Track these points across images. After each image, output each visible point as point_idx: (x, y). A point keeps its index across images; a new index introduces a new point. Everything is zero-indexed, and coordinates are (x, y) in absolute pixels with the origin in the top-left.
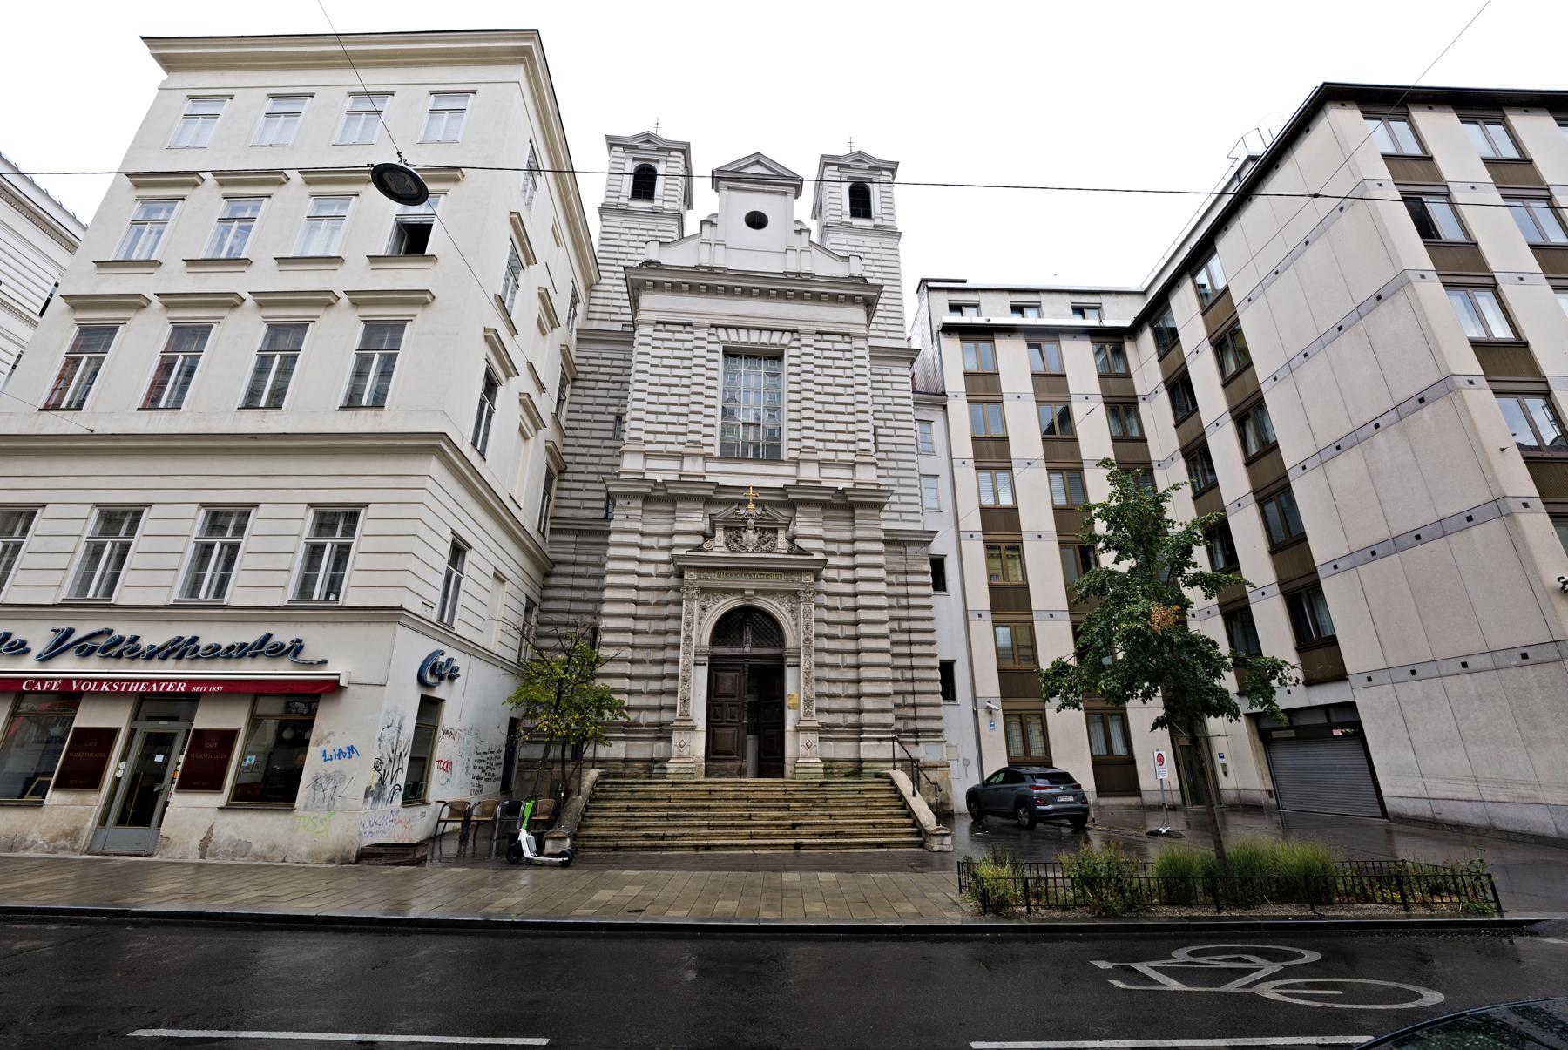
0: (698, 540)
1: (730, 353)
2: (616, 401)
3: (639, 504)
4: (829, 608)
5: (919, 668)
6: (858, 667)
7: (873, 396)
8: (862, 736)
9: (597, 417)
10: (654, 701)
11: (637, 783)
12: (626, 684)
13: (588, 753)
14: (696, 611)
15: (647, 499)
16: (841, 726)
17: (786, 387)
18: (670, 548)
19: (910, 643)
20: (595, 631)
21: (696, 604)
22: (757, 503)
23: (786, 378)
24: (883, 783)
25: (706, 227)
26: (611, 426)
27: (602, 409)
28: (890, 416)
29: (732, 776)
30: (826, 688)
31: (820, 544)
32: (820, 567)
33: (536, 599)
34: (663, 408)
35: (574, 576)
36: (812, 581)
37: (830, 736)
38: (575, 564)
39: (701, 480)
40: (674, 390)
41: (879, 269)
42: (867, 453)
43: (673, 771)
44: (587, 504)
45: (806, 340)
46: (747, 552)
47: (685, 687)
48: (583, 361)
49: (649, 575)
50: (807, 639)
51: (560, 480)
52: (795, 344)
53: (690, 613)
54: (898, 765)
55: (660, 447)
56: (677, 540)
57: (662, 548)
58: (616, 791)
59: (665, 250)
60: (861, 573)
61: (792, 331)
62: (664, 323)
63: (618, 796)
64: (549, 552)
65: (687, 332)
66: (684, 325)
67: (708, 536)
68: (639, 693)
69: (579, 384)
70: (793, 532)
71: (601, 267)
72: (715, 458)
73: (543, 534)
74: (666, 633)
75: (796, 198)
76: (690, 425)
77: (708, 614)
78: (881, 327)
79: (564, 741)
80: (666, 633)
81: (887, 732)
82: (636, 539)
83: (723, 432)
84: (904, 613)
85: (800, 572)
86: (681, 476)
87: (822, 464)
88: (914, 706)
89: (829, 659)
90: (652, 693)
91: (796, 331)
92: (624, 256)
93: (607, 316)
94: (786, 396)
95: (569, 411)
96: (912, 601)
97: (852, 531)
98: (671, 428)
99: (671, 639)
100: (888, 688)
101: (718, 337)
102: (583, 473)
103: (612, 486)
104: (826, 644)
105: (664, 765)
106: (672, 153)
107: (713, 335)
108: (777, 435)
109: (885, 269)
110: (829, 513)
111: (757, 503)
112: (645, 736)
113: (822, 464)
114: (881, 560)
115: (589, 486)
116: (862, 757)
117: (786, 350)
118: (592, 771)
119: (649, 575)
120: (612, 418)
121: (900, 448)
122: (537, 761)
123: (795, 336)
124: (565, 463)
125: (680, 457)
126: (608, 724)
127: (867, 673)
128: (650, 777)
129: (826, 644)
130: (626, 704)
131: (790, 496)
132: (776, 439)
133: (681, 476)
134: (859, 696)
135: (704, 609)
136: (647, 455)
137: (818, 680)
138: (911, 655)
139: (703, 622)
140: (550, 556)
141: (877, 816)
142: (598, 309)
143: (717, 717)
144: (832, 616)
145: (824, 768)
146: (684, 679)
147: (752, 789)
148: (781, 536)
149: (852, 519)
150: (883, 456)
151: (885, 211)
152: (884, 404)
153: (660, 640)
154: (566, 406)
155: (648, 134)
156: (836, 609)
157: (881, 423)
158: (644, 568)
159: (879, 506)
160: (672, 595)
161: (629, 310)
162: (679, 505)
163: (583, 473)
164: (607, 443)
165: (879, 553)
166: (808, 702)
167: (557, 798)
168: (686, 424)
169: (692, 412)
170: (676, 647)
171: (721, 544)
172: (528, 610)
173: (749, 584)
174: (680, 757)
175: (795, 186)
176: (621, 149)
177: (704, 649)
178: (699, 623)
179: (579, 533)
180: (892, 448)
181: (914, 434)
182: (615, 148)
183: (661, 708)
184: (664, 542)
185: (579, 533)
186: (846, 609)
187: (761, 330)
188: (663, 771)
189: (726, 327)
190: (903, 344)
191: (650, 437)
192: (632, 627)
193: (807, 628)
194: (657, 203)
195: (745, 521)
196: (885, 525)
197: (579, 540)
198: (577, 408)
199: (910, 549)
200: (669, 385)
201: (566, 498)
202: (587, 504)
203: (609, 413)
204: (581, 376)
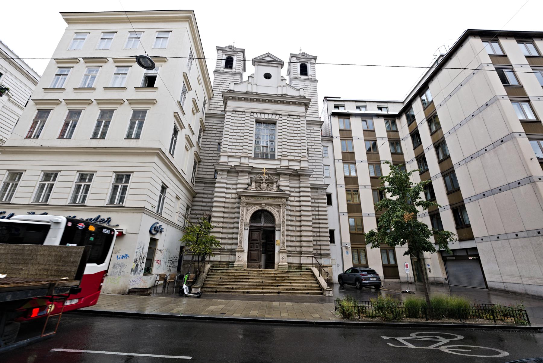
0: (246, 186)
1: (258, 122)
3: (226, 173)
4: (291, 211)
5: (322, 232)
6: (301, 231)
8: (302, 255)
9: (212, 143)
10: (230, 241)
11: (224, 270)
12: (220, 235)
13: (207, 259)
14: (245, 210)
15: (228, 172)
16: (295, 252)
17: (277, 134)
18: (236, 189)
19: (319, 223)
20: (210, 217)
21: (245, 208)
22: (266, 174)
23: (277, 131)
25: (250, 78)
26: (216, 146)
27: (214, 140)
28: (313, 144)
30: (289, 238)
31: (288, 188)
33: (190, 206)
36: (285, 201)
37: (291, 255)
38: (203, 193)
39: (247, 165)
41: (310, 93)
42: (305, 157)
43: (236, 266)
44: (208, 173)
45: (284, 118)
47: (241, 237)
48: (207, 124)
50: (283, 221)
51: (199, 165)
52: (280, 119)
53: (243, 211)
54: (314, 266)
55: (233, 154)
56: (239, 186)
57: (233, 189)
58: (216, 272)
59: (236, 86)
60: (302, 198)
61: (280, 115)
62: (235, 111)
63: (217, 274)
64: (195, 189)
65: (243, 114)
67: (249, 185)
68: (225, 238)
69: (206, 132)
71: (214, 92)
74: (234, 218)
76: (244, 146)
77: (249, 212)
78: (310, 113)
79: (199, 254)
80: (234, 218)
81: (311, 254)
82: (225, 185)
83: (255, 149)
84: (317, 213)
85: (281, 198)
86: (240, 164)
87: (289, 160)
88: (320, 245)
89: (290, 228)
90: (229, 239)
91: (281, 114)
93: (216, 109)
94: (277, 137)
95: (202, 141)
96: (320, 209)
97: (299, 184)
98: (237, 148)
99: (236, 220)
100: (311, 239)
101: (254, 116)
102: (207, 162)
103: (217, 167)
104: (290, 223)
105: (233, 263)
106: (239, 53)
107: (252, 115)
110: (292, 178)
111: (266, 174)
112: (227, 253)
113: (289, 160)
114: (309, 194)
117: (277, 121)
118: (208, 265)
120: (217, 144)
123: (281, 116)
124: (201, 159)
125: (240, 157)
126: (214, 249)
127: (304, 233)
128: (228, 268)
129: (290, 223)
130: (220, 242)
131: (278, 171)
132: (273, 152)
133: (240, 164)
135: (248, 210)
136: (229, 157)
137: (287, 235)
138: (319, 228)
139: (247, 215)
140: (195, 191)
143: (251, 247)
145: (288, 266)
147: (263, 272)
148: (275, 185)
149: (299, 180)
150: (310, 158)
151: (312, 73)
152: (311, 140)
153: (232, 221)
154: (201, 139)
155: (231, 46)
156: (293, 211)
157: (310, 147)
158: (227, 196)
160: (237, 205)
161: (223, 107)
162: (240, 174)
163: (207, 162)
164: (215, 152)
165: (308, 192)
166: (283, 243)
170: (238, 223)
171: (254, 187)
172: (187, 209)
173: (263, 202)
176: (221, 51)
177: (247, 224)
178: (246, 215)
179: (205, 183)
180: (314, 155)
182: (219, 51)
183: (232, 244)
184: (234, 187)
185: (205, 183)
186: (297, 211)
187: (269, 114)
188: (233, 266)
189: (257, 113)
190: (318, 119)
191: (230, 150)
193: (283, 217)
194: (234, 70)
195: (262, 180)
196: (311, 182)
198: (205, 140)
199: (320, 191)
201: (201, 171)
202: (208, 173)
203: (216, 142)
204: (207, 129)
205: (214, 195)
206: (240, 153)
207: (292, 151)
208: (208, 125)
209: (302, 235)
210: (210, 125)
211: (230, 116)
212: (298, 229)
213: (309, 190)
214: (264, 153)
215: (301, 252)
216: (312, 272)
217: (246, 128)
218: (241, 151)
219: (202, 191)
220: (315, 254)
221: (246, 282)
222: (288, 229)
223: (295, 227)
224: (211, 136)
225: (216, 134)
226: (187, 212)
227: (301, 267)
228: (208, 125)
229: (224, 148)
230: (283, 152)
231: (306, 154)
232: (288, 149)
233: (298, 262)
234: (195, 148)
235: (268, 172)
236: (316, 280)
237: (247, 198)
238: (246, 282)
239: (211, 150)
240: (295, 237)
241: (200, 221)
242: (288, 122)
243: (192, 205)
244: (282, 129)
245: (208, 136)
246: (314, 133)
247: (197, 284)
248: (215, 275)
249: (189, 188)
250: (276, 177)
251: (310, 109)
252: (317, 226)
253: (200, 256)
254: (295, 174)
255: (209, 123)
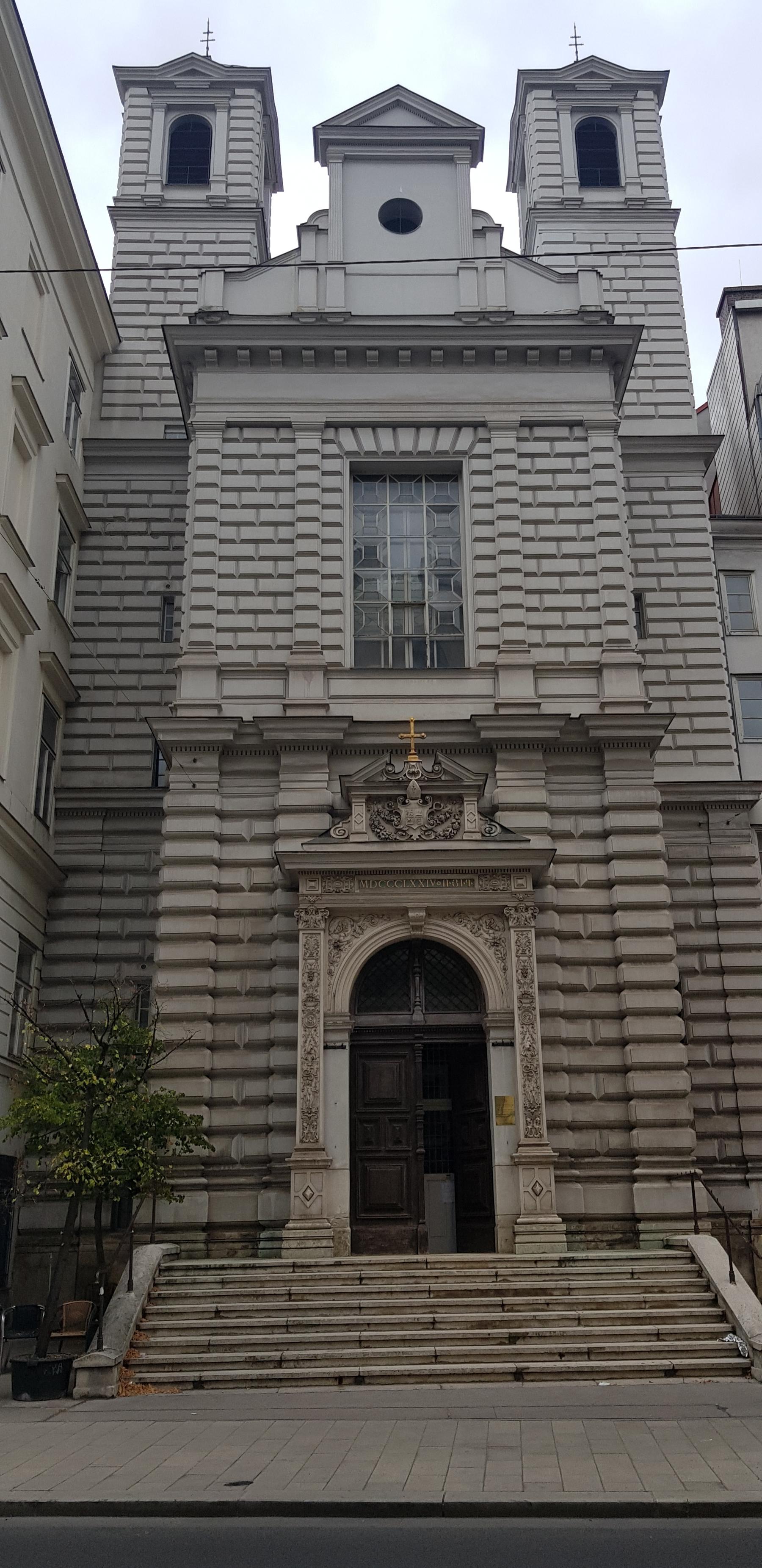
0: (322, 821)
2: (161, 570)
3: (213, 761)
4: (563, 937)
5: (742, 1040)
6: (623, 1043)
7: (629, 504)
8: (637, 1171)
9: (130, 601)
10: (255, 1117)
11: (231, 1267)
12: (203, 1088)
13: (143, 1216)
14: (323, 951)
15: (226, 751)
16: (597, 1154)
17: (469, 532)
18: (272, 838)
19: (724, 994)
20: (144, 986)
21: (322, 938)
22: (424, 750)
23: (468, 515)
24: (675, 1258)
25: (310, 238)
26: (155, 617)
27: (138, 586)
28: (668, 567)
29: (401, 1251)
30: (564, 1084)
31: (542, 820)
32: (543, 863)
33: (36, 939)
34: (247, 585)
35: (102, 892)
36: (530, 888)
37: (576, 1172)
38: (102, 871)
39: (321, 712)
40: (266, 550)
41: (638, 285)
42: (623, 646)
43: (294, 1244)
44: (119, 761)
45: (502, 440)
46: (410, 840)
47: (310, 1089)
48: (98, 498)
49: (235, 889)
50: (525, 995)
51: (68, 721)
52: (480, 448)
53: (312, 955)
54: (705, 1224)
55: (245, 656)
56: (284, 823)
57: (258, 840)
58: (194, 1283)
59: (236, 287)
60: (620, 869)
61: (475, 425)
62: (241, 426)
63: (197, 1291)
64: (57, 852)
65: (283, 440)
66: (278, 426)
67: (338, 814)
68: (228, 1103)
69: (92, 541)
70: (492, 798)
71: (119, 320)
72: (346, 671)
73: (43, 821)
74: (271, 992)
75: (474, 165)
76: (298, 613)
77: (345, 955)
78: (645, 397)
79: (100, 1196)
80: (271, 992)
81: (683, 1164)
82: (211, 824)
83: (357, 624)
84: (709, 938)
85: (506, 873)
86: (285, 706)
87: (540, 670)
88: (737, 1112)
89: (567, 1030)
90: (250, 1103)
91: (483, 424)
92: (160, 296)
93: (134, 412)
94: (470, 549)
95: (78, 593)
96: (724, 915)
97: (600, 792)
98: (264, 621)
99: (281, 1003)
100: (680, 1081)
101: (340, 445)
102: (109, 704)
103: (164, 731)
104: (561, 1002)
105: (277, 1234)
106: (238, 92)
107: (331, 442)
108: (455, 622)
109: (649, 284)
110: (557, 761)
111: (424, 750)
112: (242, 1180)
113: (540, 670)
114: (656, 843)
115: (121, 728)
116: (637, 1211)
117: (465, 461)
118: (151, 1247)
119: (235, 889)
120: (156, 601)
121: (690, 627)
122: (53, 1232)
123: (482, 433)
124: (77, 688)
125: (282, 671)
126: (176, 1160)
127: (639, 1054)
128: (254, 1256)
129: (561, 1002)
130: (205, 1124)
131: (484, 734)
132: (454, 629)
133: (285, 706)
134: (627, 1098)
135: (337, 946)
136: (223, 672)
137: (549, 1070)
138: (726, 1017)
139: (337, 970)
140: (57, 858)
141: (663, 1319)
142: (119, 398)
143: (369, 1143)
144: (570, 950)
145: (568, 1233)
146: (307, 1075)
147: (435, 1272)
148: (470, 809)
149: (600, 770)
150: (658, 644)
151: (644, 170)
152: (656, 546)
153: (261, 1006)
154: (71, 584)
155: (192, 58)
156: (577, 937)
157: (652, 582)
158: (228, 877)
159: (652, 745)
160: (278, 924)
161: (174, 398)
162: (285, 760)
163: (109, 704)
164: (150, 648)
165: (651, 831)
166: (532, 1111)
167: (95, 1296)
168: (290, 576)
169: (299, 590)
170: (291, 1017)
171: (363, 827)
172: (23, 960)
174: (305, 1218)
175: (469, 144)
176: (144, 91)
177: (339, 1020)
178: (330, 973)
179: (108, 814)
180: (674, 628)
181: (715, 598)
182: (133, 90)
183: (267, 1130)
184: (262, 827)
185: (108, 814)
186: (596, 936)
187: (418, 426)
188: (276, 1244)
189: (354, 426)
190: (690, 428)
191: (226, 639)
192: (211, 985)
193: (525, 974)
194: (217, 189)
195: (403, 784)
196: (662, 775)
197: (106, 828)
198: (91, 585)
199: (716, 818)
200: (255, 648)
201: (82, 753)
202: (119, 761)
203: (151, 593)
204: (96, 526)
205: (162, 856)
206: (279, 647)
207: (555, 618)
208: (100, 505)
209: (629, 1062)
210: (110, 506)
211: (216, 451)
212: (609, 1030)
213: (654, 819)
214: (408, 639)
215: (633, 1153)
216: (693, 1259)
217: (303, 510)
218: (283, 638)
219: (96, 860)
220: (714, 1160)
221: (349, 1326)
222: (552, 1033)
223: (589, 1022)
224: (124, 563)
225: (146, 549)
226: (24, 976)
227: (638, 1233)
228: (100, 505)
229: (195, 590)
230: (600, 505)
231: (626, 632)
232: (529, 609)
233: (617, 1208)
234: (40, 640)
235: (430, 740)
236: (714, 1302)
237: (333, 886)
238: (349, 1326)
239: (124, 640)
240: (592, 1076)
241: (99, 1017)
242: (526, 463)
243: (45, 934)
244: (491, 506)
245: (106, 563)
246: (669, 503)
247: (100, 1348)
248: (186, 1297)
249: (22, 845)
250: (473, 765)
251: (642, 371)
252: (715, 1006)
253: (104, 1205)
254: (574, 738)
255: (105, 492)
